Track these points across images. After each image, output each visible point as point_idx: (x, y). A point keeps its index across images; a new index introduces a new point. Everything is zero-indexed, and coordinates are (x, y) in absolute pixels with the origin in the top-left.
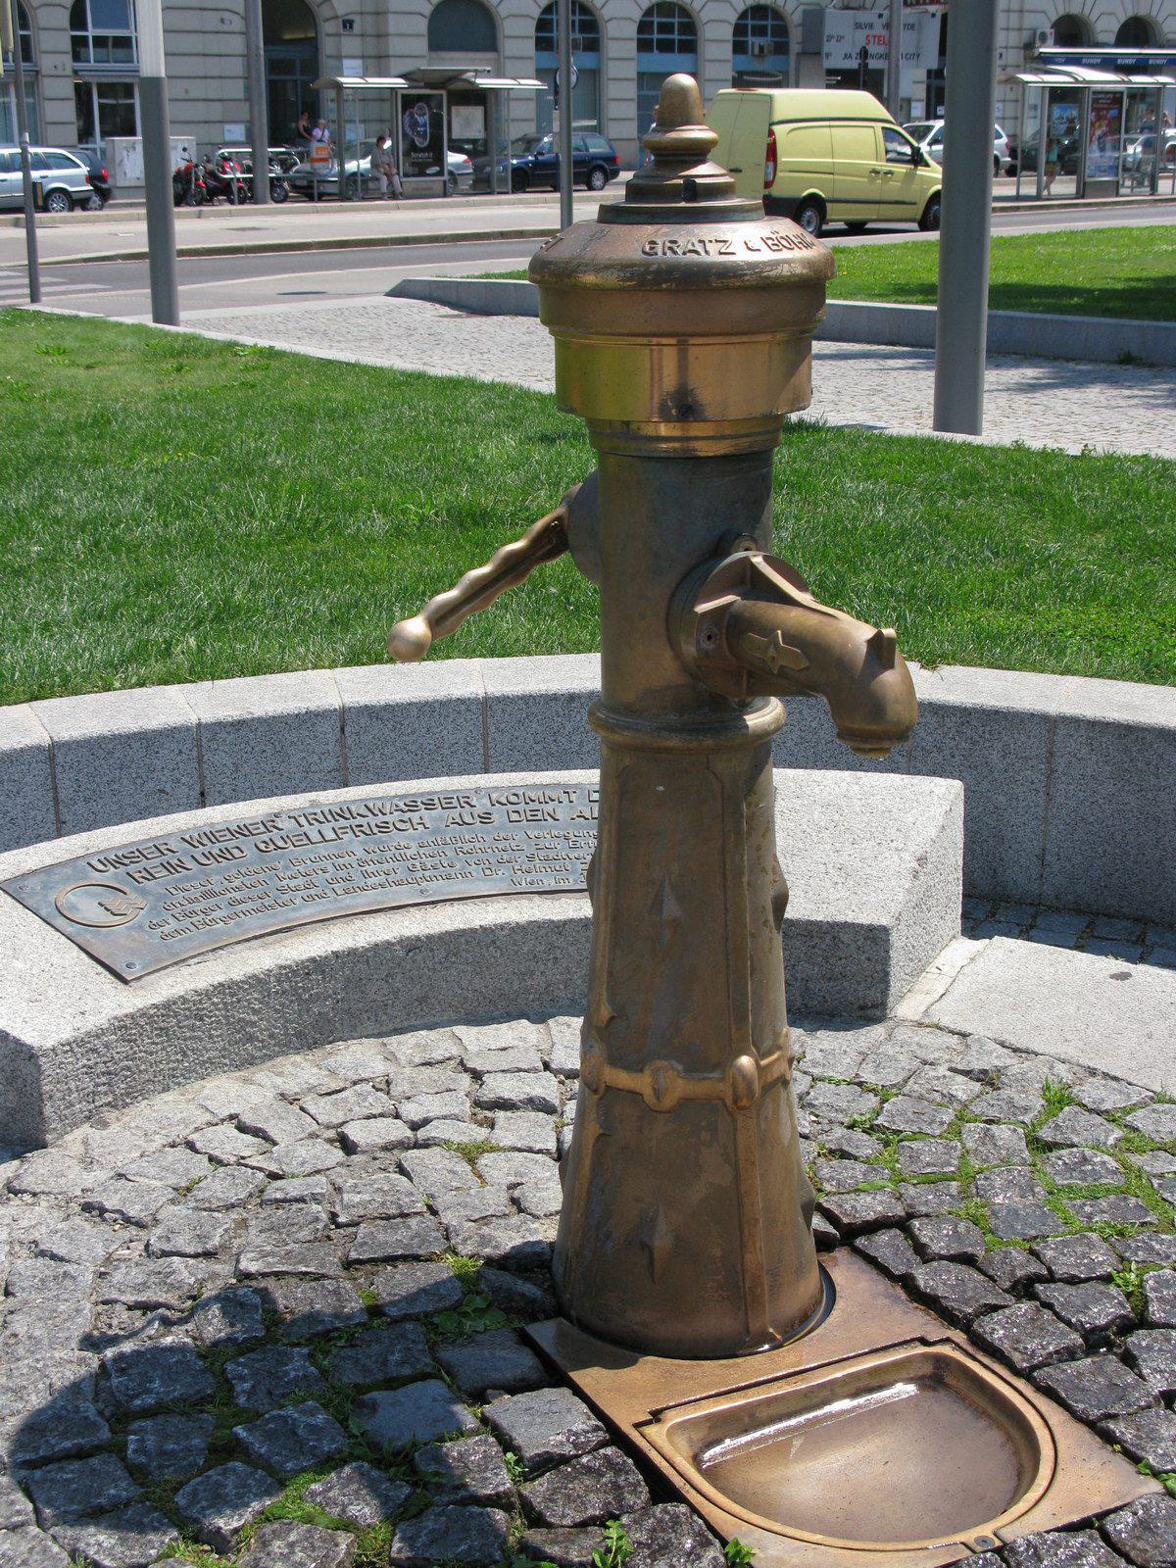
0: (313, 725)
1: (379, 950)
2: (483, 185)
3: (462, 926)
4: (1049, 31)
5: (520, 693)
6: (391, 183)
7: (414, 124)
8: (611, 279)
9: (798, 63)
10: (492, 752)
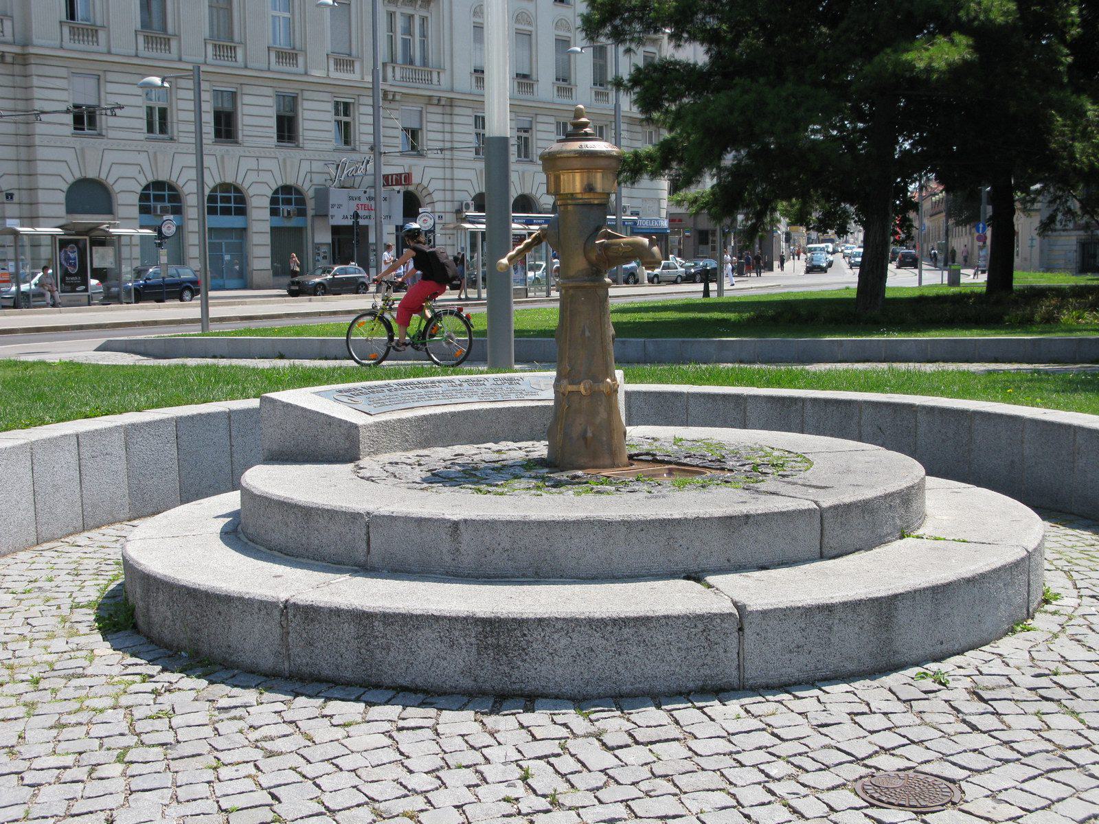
1: (443, 415)
2: (110, 298)
4: (471, 202)
6: (52, 297)
7: (68, 259)
8: (572, 155)
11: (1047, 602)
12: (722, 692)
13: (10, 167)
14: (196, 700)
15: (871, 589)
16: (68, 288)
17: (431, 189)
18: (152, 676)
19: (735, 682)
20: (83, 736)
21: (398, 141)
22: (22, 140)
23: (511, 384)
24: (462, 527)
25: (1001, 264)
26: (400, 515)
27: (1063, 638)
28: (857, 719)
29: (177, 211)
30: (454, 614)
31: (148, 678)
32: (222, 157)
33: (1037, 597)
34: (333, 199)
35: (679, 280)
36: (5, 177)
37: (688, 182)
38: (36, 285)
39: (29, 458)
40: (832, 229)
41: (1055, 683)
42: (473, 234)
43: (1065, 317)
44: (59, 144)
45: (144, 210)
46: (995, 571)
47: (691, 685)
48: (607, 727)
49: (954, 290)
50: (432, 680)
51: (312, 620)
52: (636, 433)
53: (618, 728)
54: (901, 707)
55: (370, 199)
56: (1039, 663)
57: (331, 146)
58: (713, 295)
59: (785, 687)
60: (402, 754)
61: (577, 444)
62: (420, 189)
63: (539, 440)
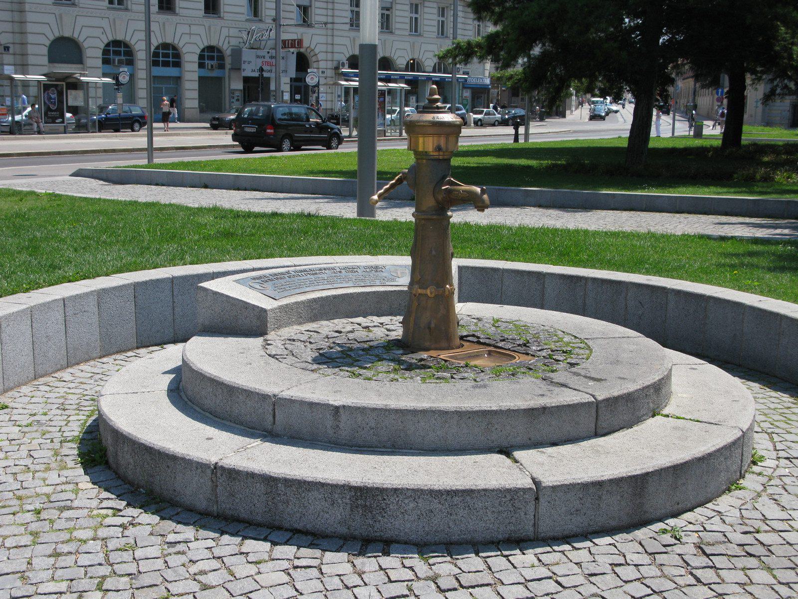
2: (81, 128)
4: (346, 62)
6: (38, 127)
7: (50, 98)
8: (427, 124)
9: (229, 73)
11: (754, 463)
12: (521, 542)
13: (8, 27)
14: (151, 534)
15: (630, 469)
16: (50, 120)
17: (317, 51)
18: (120, 510)
19: (531, 534)
20: (72, 565)
21: (293, 16)
22: (15, 7)
23: (376, 271)
24: (341, 411)
25: (734, 122)
26: (296, 399)
27: (764, 499)
28: (617, 569)
29: (130, 62)
30: (335, 483)
31: (117, 511)
32: (164, 24)
33: (748, 460)
34: (244, 58)
35: (497, 123)
36: (3, 34)
37: (506, 66)
38: (26, 116)
39: (29, 318)
40: (610, 96)
41: (757, 540)
42: (347, 90)
43: (779, 177)
44: (43, 10)
45: (106, 61)
46: (719, 450)
47: (500, 537)
48: (441, 572)
49: (698, 143)
50: (318, 527)
51: (234, 479)
52: (463, 309)
53: (448, 572)
54: (646, 559)
55: (271, 57)
56: (747, 521)
57: (244, 17)
58: (521, 140)
59: (567, 539)
60: (297, 590)
61: (425, 334)
62: (309, 50)
63: (395, 316)
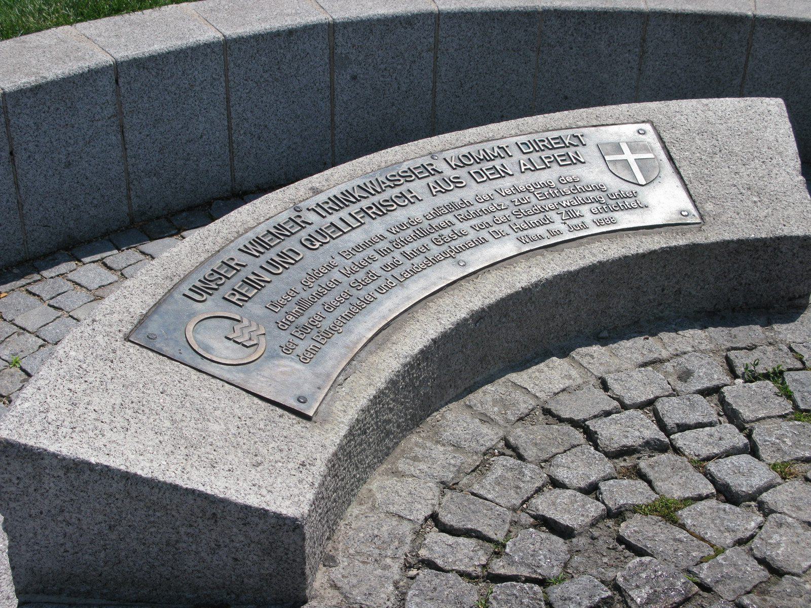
0: (95, 81)
3: (509, 291)
5: (252, 33)
10: (232, 83)
